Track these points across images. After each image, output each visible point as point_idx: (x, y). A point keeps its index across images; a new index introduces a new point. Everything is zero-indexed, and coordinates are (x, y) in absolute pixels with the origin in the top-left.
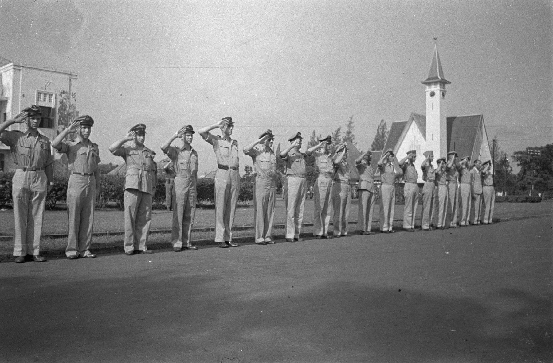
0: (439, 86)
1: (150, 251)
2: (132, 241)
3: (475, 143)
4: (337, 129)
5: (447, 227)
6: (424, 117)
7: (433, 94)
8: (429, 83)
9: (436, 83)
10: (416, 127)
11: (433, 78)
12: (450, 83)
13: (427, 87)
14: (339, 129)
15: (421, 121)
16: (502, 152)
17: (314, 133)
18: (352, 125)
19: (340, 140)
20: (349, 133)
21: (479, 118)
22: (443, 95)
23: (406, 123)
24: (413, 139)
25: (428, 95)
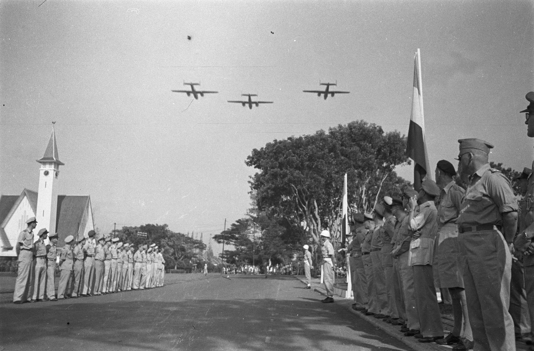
0: (53, 166)
6: (36, 194)
7: (46, 173)
8: (44, 161)
9: (51, 163)
12: (63, 164)
13: (42, 166)
15: (33, 196)
21: (87, 198)
22: (56, 175)
25: (42, 173)
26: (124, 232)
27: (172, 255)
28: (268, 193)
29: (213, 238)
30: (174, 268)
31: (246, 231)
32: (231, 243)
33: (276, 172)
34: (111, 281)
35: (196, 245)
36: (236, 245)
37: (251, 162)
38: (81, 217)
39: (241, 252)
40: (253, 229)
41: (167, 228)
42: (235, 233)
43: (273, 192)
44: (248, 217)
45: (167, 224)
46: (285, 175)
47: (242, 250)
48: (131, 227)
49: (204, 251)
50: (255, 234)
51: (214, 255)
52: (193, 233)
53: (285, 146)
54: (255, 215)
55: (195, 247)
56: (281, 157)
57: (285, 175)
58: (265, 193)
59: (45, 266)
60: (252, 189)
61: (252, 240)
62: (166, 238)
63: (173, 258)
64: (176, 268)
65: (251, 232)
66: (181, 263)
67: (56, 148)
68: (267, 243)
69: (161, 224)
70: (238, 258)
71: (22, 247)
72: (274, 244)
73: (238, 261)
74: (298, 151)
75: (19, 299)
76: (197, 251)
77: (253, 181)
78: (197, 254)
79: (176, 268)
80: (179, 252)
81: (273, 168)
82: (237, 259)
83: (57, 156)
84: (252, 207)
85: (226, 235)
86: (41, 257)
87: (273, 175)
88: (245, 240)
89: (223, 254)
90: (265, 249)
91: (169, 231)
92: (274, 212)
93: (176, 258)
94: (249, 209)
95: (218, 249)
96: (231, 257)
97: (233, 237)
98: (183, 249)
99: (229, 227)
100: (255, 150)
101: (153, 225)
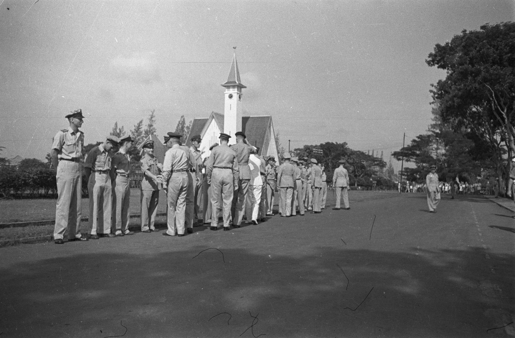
0: (236, 89)
1: (157, 230)
2: (148, 223)
3: (265, 141)
4: (139, 122)
5: (291, 215)
6: (223, 116)
7: (231, 96)
8: (228, 86)
9: (234, 87)
10: (216, 124)
11: (231, 82)
12: (245, 87)
13: (226, 90)
14: (141, 122)
15: (220, 118)
16: (282, 148)
17: (116, 124)
18: (153, 119)
19: (142, 132)
20: (150, 126)
21: (269, 118)
22: (240, 98)
23: (207, 120)
24: (213, 135)
25: (227, 96)
26: (306, 151)
27: (352, 172)
28: (454, 102)
29: (392, 155)
30: (354, 185)
31: (428, 147)
32: (411, 160)
33: (466, 70)
34: (196, 208)
35: (376, 163)
36: (417, 162)
37: (433, 61)
38: (264, 137)
39: (423, 169)
40: (435, 146)
41: (347, 146)
42: (416, 150)
43: (459, 100)
44: (430, 133)
45: (347, 142)
46: (478, 73)
47: (424, 167)
48: (312, 146)
49: (385, 169)
50: (438, 151)
51: (395, 173)
52: (373, 151)
53: (477, 37)
54: (438, 131)
55: (375, 165)
56: (472, 51)
57: (478, 73)
58: (450, 102)
59: (109, 184)
60: (434, 99)
61: (435, 157)
62: (346, 156)
63: (353, 176)
64: (356, 185)
65: (434, 149)
66: (361, 180)
67: (238, 73)
68: (452, 160)
69: (340, 142)
70: (419, 175)
71: (59, 156)
72: (460, 162)
73: (419, 179)
74: (495, 43)
75: (61, 237)
76: (377, 168)
77: (435, 90)
78: (377, 172)
79: (356, 185)
80: (363, 170)
81: (461, 64)
82: (418, 176)
83: (239, 79)
84: (434, 122)
85: (406, 152)
86: (100, 172)
87: (462, 73)
88: (427, 157)
89: (402, 171)
90: (449, 166)
91: (349, 149)
92: (461, 123)
93: (356, 176)
94: (431, 125)
95: (398, 166)
96: (412, 174)
97: (414, 154)
98: (363, 167)
99: (408, 143)
100: (438, 46)
101: (333, 144)
